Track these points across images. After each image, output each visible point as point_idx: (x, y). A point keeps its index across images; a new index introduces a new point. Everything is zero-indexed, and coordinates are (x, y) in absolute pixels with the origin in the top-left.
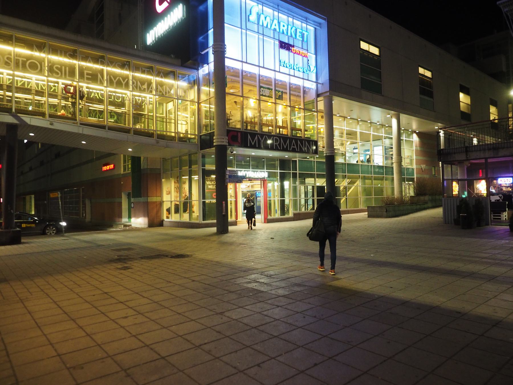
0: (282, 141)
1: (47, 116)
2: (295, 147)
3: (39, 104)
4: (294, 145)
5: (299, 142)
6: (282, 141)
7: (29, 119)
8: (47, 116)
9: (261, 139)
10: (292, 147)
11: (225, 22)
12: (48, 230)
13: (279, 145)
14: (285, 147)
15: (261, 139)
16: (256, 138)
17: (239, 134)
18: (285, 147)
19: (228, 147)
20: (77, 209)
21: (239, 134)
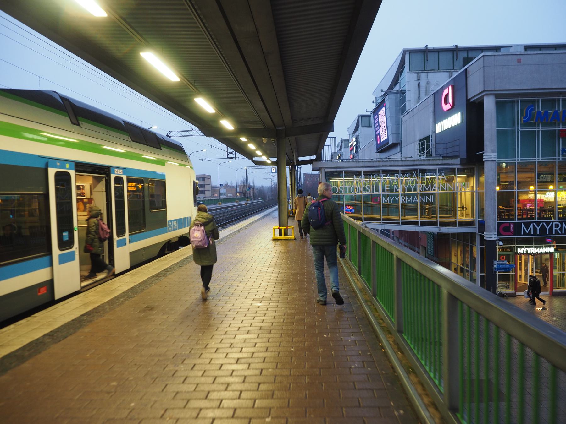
17: (512, 225)
21: (512, 225)
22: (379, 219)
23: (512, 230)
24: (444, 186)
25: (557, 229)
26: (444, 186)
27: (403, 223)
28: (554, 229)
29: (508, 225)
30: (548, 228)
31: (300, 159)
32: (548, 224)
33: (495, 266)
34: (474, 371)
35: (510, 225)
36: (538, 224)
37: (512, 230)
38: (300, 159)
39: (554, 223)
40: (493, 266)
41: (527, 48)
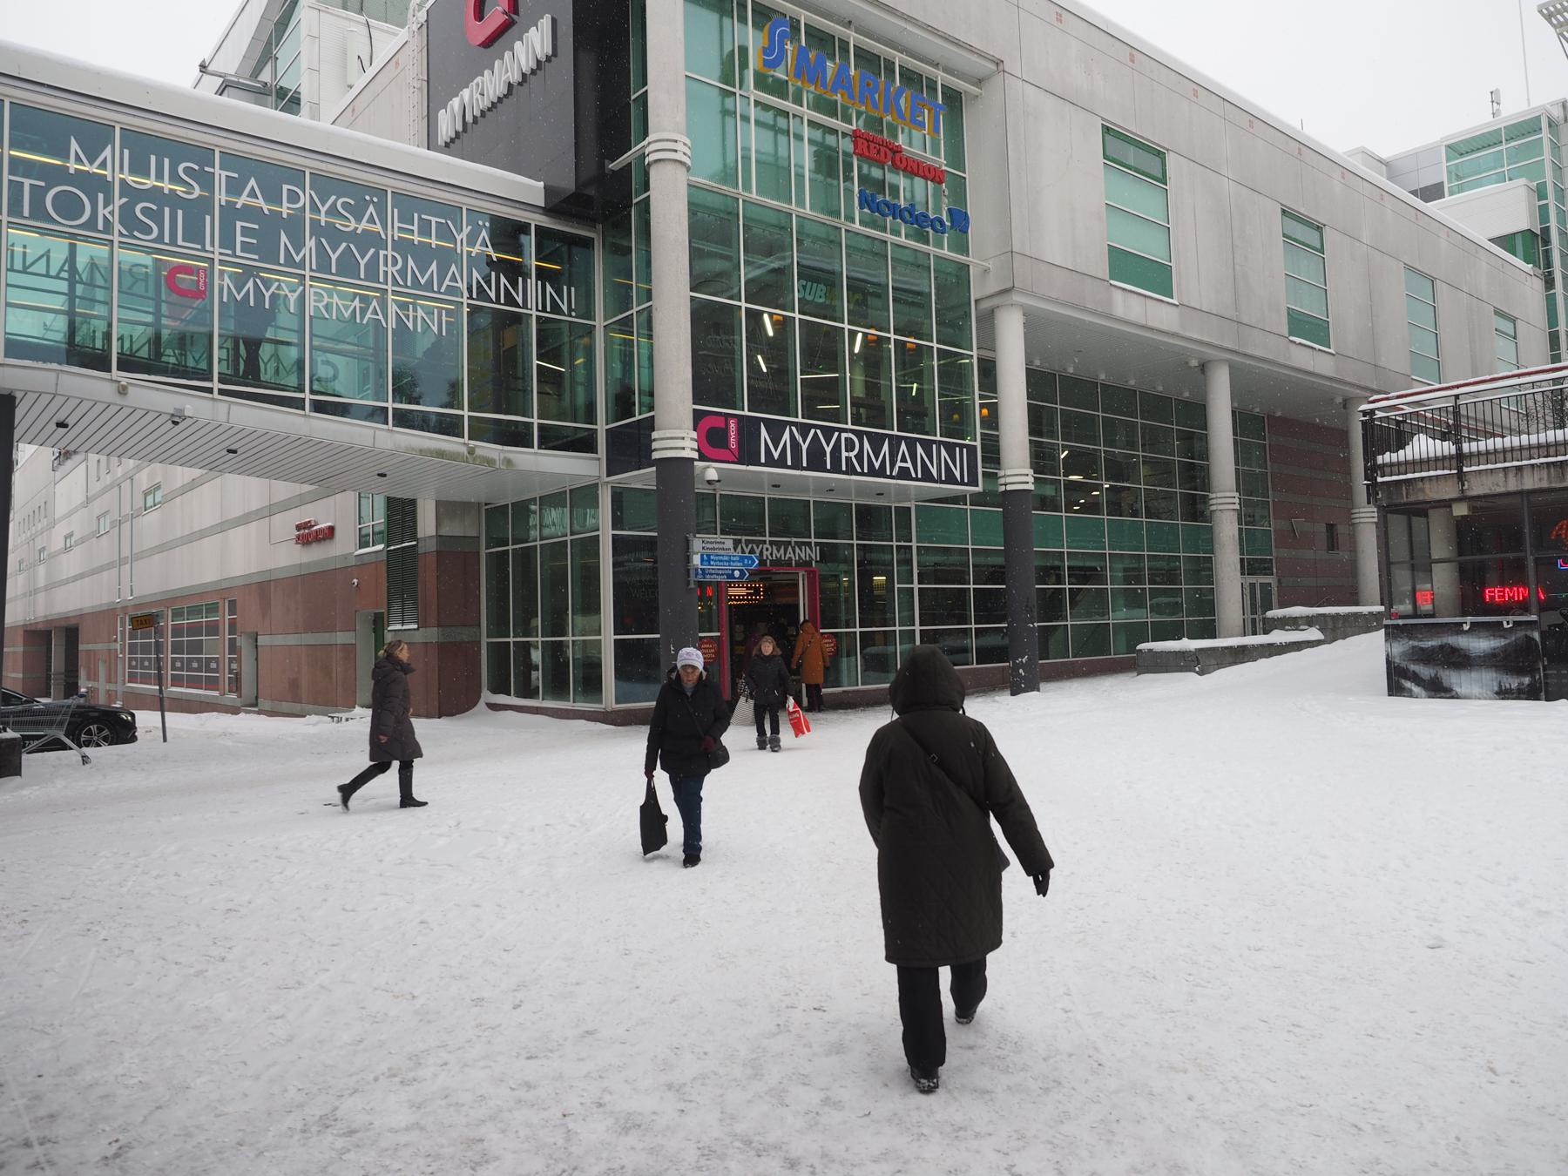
0: (411, 262)
1: (35, 1143)
2: (909, 465)
3: (139, 168)
4: (904, 460)
5: (920, 450)
6: (411, 262)
7: (54, 374)
8: (35, 1143)
9: (800, 440)
10: (899, 464)
11: (1525, 107)
12: (100, 730)
13: (859, 457)
14: (877, 465)
15: (800, 440)
16: (786, 436)
17: (732, 425)
18: (877, 465)
19: (695, 455)
20: (213, 665)
21: (732, 425)
22: (210, 390)
23: (733, 443)
24: (488, 283)
25: (852, 454)
26: (488, 283)
27: (319, 407)
28: (844, 454)
29: (720, 423)
30: (828, 450)
31: (180, 212)
32: (828, 433)
33: (696, 560)
34: (1482, 445)
35: (727, 424)
36: (805, 430)
37: (733, 443)
38: (180, 212)
39: (844, 435)
40: (688, 559)
41: (1457, 149)
